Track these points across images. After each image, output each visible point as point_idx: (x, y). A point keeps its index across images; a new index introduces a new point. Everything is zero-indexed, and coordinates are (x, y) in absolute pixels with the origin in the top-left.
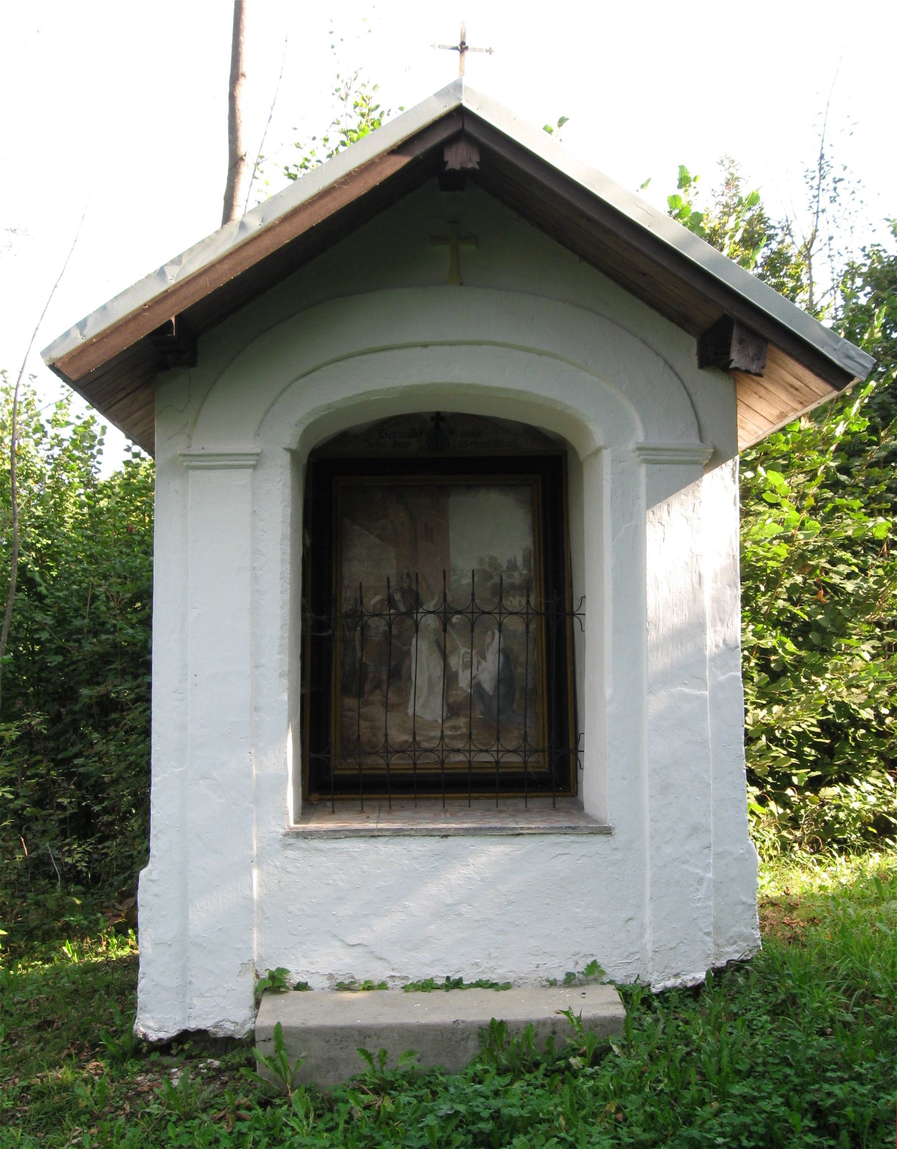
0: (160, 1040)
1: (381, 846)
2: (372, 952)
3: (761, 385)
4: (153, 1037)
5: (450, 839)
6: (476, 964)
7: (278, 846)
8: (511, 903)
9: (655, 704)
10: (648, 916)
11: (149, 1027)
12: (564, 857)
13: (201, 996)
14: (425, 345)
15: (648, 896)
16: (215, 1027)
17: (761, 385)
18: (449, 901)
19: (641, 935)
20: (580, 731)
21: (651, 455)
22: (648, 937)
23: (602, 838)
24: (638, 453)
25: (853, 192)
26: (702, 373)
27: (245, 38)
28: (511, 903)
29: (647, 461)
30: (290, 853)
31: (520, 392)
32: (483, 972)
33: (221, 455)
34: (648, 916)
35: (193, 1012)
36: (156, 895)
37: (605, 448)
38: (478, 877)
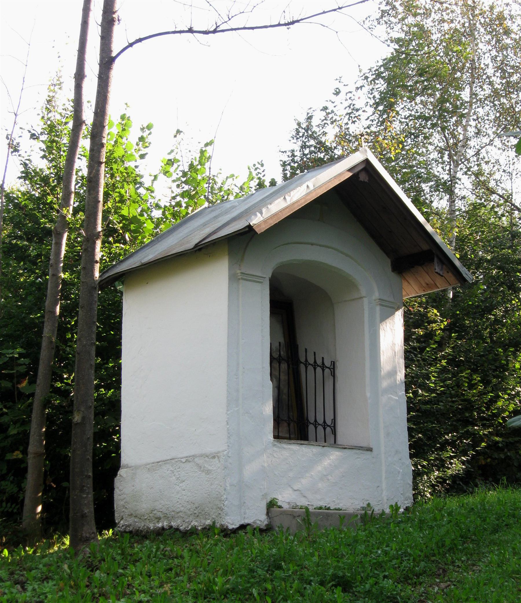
0: (233, 528)
1: (304, 449)
2: (302, 494)
3: (407, 281)
4: (231, 527)
5: (325, 448)
6: (334, 501)
7: (271, 445)
8: (343, 476)
9: (384, 399)
10: (384, 486)
11: (229, 523)
12: (359, 459)
13: (249, 509)
14: (312, 244)
15: (384, 477)
16: (253, 523)
17: (407, 281)
18: (325, 473)
19: (382, 494)
20: (276, 389)
21: (382, 303)
22: (385, 493)
23: (369, 452)
24: (378, 301)
25: (179, 132)
26: (393, 273)
27: (122, 54)
28: (343, 476)
29: (381, 305)
30: (275, 449)
31: (340, 270)
32: (336, 505)
33: (253, 275)
34: (384, 486)
35: (246, 516)
36: (230, 463)
37: (364, 297)
38: (333, 464)
